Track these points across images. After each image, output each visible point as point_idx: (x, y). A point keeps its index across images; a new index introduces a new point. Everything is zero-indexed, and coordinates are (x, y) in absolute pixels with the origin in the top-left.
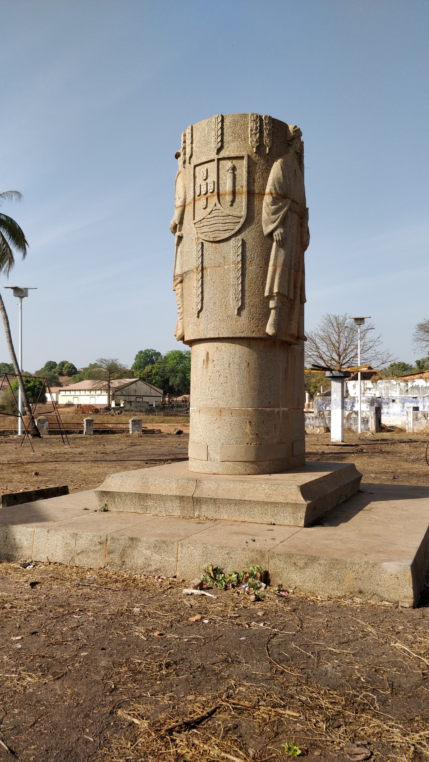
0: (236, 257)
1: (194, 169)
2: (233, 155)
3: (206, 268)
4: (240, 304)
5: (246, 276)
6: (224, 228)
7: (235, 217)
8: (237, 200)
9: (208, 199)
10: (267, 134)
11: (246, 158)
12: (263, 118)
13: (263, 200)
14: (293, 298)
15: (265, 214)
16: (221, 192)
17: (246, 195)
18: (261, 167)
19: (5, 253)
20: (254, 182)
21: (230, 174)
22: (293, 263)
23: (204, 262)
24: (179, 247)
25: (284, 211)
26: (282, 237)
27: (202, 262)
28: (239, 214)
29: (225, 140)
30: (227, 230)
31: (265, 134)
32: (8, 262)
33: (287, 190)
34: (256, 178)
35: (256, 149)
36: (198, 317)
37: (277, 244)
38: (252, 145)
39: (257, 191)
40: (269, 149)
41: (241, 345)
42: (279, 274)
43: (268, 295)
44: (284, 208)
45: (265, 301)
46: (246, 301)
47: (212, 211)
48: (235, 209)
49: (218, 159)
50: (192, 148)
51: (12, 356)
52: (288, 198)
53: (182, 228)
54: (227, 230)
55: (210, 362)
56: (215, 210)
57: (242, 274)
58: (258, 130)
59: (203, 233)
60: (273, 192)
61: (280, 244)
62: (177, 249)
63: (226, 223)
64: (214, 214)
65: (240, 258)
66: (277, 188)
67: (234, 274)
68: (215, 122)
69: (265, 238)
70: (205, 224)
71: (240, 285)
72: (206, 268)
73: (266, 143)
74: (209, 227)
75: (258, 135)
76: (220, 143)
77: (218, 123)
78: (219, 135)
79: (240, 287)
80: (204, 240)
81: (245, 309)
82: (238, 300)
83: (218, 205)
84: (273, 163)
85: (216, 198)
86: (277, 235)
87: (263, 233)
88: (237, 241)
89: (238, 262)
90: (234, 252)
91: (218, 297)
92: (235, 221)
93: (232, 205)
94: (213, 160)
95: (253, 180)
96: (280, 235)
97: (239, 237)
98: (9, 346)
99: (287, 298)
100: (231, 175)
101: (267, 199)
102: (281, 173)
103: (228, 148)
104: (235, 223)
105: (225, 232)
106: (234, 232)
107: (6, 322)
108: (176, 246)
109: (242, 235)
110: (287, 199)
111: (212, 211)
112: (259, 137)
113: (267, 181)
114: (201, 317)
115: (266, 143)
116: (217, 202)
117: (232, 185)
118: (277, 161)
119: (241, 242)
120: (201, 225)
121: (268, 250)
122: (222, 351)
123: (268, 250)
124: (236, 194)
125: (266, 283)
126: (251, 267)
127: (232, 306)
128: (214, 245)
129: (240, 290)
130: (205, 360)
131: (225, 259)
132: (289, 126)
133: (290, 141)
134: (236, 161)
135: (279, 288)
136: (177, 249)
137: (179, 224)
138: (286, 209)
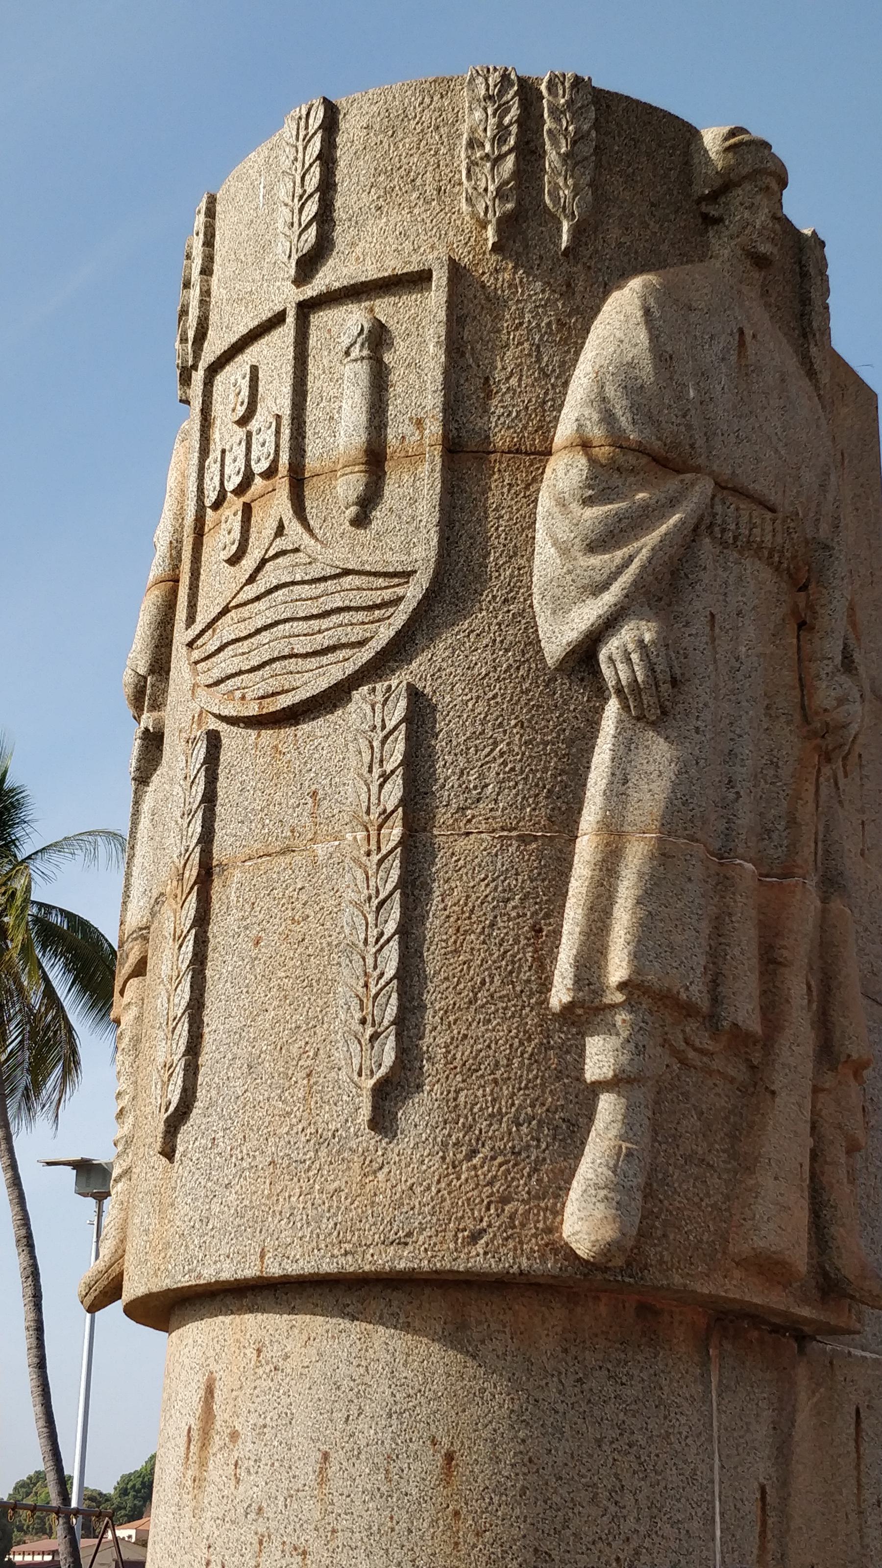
0: (374, 789)
2: (371, 272)
4: (389, 1058)
5: (431, 892)
7: (376, 574)
8: (391, 489)
10: (565, 158)
11: (440, 278)
12: (543, 88)
13: (537, 479)
14: (755, 1025)
16: (312, 463)
17: (438, 460)
18: (528, 317)
19: (49, 1040)
20: (489, 395)
22: (745, 818)
23: (219, 834)
24: (151, 788)
25: (663, 529)
26: (651, 669)
27: (207, 838)
28: (395, 561)
29: (340, 214)
31: (552, 157)
32: (58, 1071)
33: (689, 427)
34: (498, 375)
35: (499, 231)
36: (168, 1152)
37: (625, 707)
38: (474, 215)
39: (501, 438)
40: (577, 232)
41: (407, 1327)
42: (641, 875)
43: (566, 998)
44: (664, 517)
45: (557, 1039)
46: (428, 1040)
48: (379, 536)
51: (42, 1423)
52: (697, 469)
53: (165, 691)
55: (217, 1441)
56: (276, 556)
57: (403, 884)
58: (512, 141)
59: (217, 683)
60: (596, 433)
61: (640, 706)
62: (137, 803)
64: (269, 577)
65: (394, 792)
66: (618, 412)
67: (362, 885)
68: (293, 141)
71: (394, 944)
73: (556, 199)
75: (510, 162)
76: (313, 230)
77: (307, 141)
78: (309, 191)
79: (392, 952)
80: (219, 717)
81: (419, 1087)
82: (374, 1037)
83: (294, 527)
84: (604, 300)
86: (617, 657)
88: (380, 698)
89: (386, 816)
90: (367, 759)
92: (377, 597)
93: (361, 521)
94: (278, 319)
95: (479, 382)
96: (635, 657)
97: (399, 680)
98: (35, 1383)
99: (712, 1021)
101: (561, 473)
102: (643, 336)
103: (353, 244)
105: (324, 660)
106: (365, 655)
107: (30, 1292)
108: (132, 785)
110: (688, 477)
112: (517, 174)
113: (566, 384)
114: (184, 1154)
115: (556, 199)
117: (363, 418)
118: (620, 287)
119: (403, 703)
121: (570, 743)
122: (288, 1366)
123: (570, 743)
124: (389, 466)
125: (557, 933)
126: (462, 842)
127: (343, 1075)
128: (268, 736)
129: (390, 972)
130: (195, 1434)
131: (317, 804)
132: (703, 132)
133: (714, 197)
134: (392, 299)
135: (637, 956)
136: (137, 803)
138: (676, 518)
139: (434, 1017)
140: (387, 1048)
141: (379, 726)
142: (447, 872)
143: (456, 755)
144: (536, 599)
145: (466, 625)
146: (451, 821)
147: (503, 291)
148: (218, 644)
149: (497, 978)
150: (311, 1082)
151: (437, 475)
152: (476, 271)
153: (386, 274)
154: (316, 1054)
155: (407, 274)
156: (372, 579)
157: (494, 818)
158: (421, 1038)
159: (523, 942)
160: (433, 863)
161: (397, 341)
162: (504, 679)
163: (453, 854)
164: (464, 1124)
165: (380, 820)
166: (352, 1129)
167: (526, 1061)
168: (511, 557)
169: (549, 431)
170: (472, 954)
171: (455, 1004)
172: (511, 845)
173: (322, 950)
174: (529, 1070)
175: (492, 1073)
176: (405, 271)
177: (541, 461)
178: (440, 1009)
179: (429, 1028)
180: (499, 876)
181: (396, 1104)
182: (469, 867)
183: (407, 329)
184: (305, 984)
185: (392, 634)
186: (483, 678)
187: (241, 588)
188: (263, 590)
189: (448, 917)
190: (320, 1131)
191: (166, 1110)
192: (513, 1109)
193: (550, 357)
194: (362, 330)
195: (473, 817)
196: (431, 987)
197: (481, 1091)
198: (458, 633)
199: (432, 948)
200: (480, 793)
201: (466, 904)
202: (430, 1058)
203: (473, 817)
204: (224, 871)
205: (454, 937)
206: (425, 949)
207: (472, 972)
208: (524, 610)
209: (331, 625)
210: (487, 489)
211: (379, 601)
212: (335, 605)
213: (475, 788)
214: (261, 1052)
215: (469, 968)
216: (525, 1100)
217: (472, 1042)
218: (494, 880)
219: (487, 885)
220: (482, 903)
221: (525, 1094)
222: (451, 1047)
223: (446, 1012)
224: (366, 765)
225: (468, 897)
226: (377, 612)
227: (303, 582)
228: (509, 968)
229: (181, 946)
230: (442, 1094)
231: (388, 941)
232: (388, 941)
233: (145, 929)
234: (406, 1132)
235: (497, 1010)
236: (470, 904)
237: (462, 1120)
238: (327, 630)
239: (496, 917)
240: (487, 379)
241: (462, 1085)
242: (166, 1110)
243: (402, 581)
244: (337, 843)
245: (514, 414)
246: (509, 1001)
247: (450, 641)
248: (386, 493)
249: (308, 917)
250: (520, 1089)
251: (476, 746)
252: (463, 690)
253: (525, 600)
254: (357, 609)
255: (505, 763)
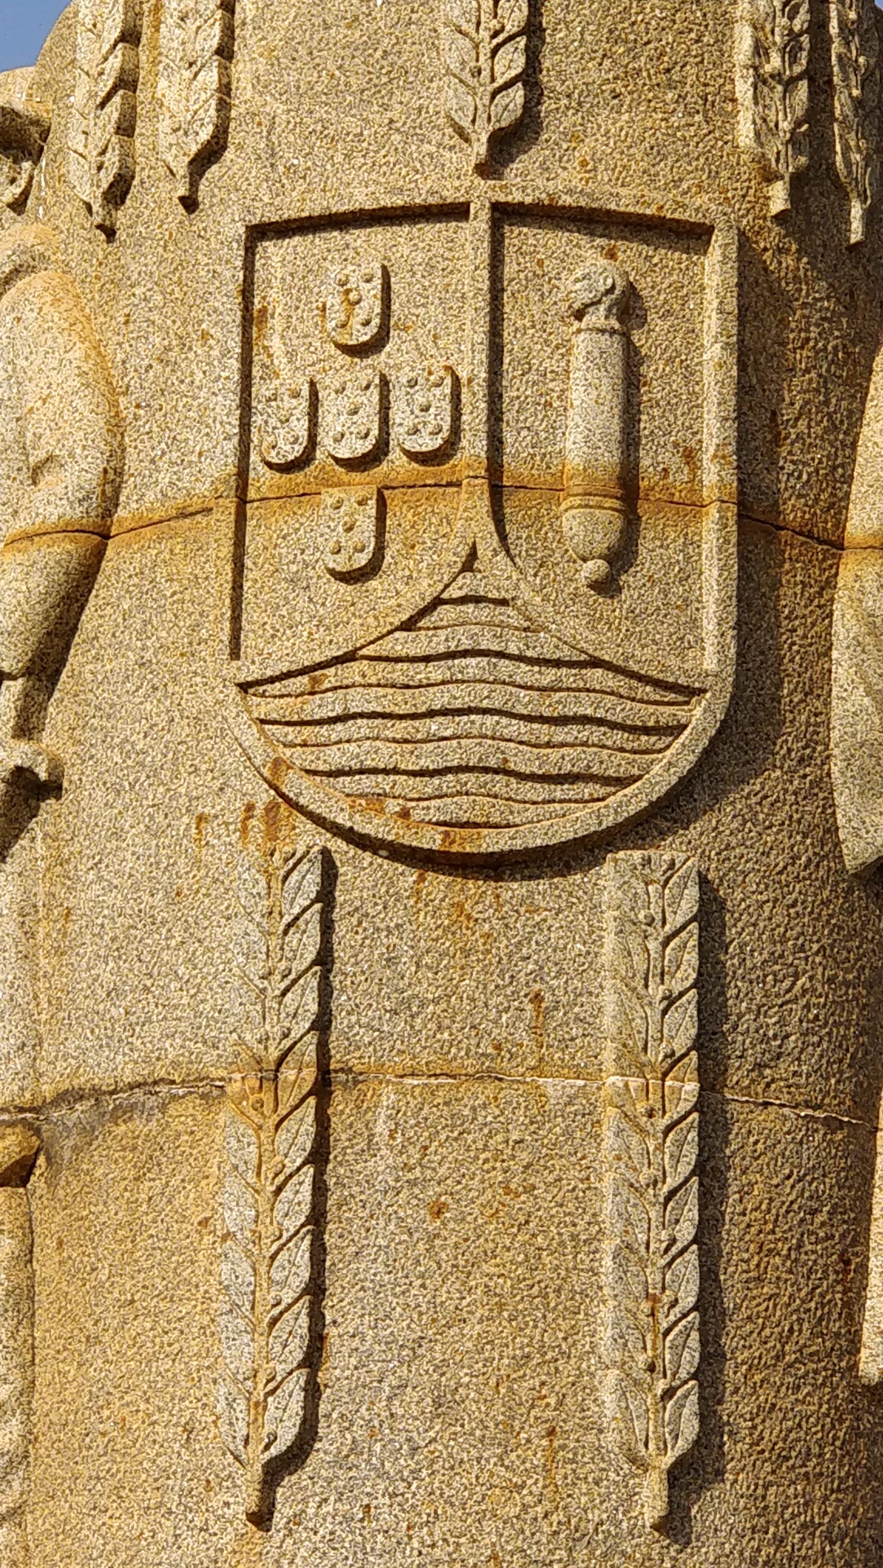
1: (250, 251)
3: (356, 1079)
4: (690, 1428)
5: (724, 1186)
6: (554, 755)
8: (646, 545)
9: (393, 507)
10: (858, 103)
13: (830, 584)
15: (860, 699)
18: (814, 332)
21: (604, 340)
23: (340, 1022)
30: (572, 778)
31: (841, 105)
34: (788, 414)
40: (869, 217)
47: (438, 602)
49: (496, 207)
50: (225, 89)
54: (572, 778)
56: (463, 600)
63: (563, 721)
69: (850, 891)
70: (357, 701)
71: (692, 1256)
72: (356, 1079)
73: (848, 163)
74: (400, 729)
78: (511, 28)
81: (720, 1473)
82: (668, 1393)
85: (484, 505)
87: (837, 844)
91: (484, 1342)
92: (650, 715)
100: (613, 346)
103: (576, 138)
104: (646, 730)
105: (559, 792)
109: (693, 832)
111: (438, 602)
113: (854, 445)
114: (297, 1519)
116: (487, 544)
119: (692, 892)
120: (330, 704)
127: (610, 1439)
129: (688, 1299)
137: (28, 672)
139: (735, 1373)
140: (686, 1411)
141: (658, 917)
142: (743, 1159)
143: (751, 982)
144: (836, 768)
145: (758, 787)
146: (747, 1082)
147: (787, 284)
148: (339, 710)
149: (806, 1325)
150: (556, 1444)
151: (733, 550)
152: (757, 242)
153: (648, 212)
154: (560, 1403)
155: (678, 221)
156: (634, 683)
157: (798, 1086)
158: (720, 1402)
159: (832, 1277)
160: (727, 1143)
161: (652, 316)
162: (804, 878)
163: (750, 1132)
164: (774, 1534)
165: (666, 1065)
166: (625, 1525)
167: (838, 1452)
168: (806, 695)
169: (840, 513)
170: (778, 1287)
171: (760, 1358)
172: (816, 1131)
173: (562, 1244)
174: (842, 1466)
175: (804, 1465)
176: (676, 216)
177: (834, 556)
178: (743, 1363)
179: (730, 1388)
180: (805, 1175)
181: (688, 1495)
182: (769, 1155)
183: (666, 301)
184: (535, 1291)
185: (674, 780)
186: (780, 873)
187: (390, 632)
188: (442, 649)
189: (749, 1226)
190: (573, 1521)
191: (267, 1447)
192: (826, 1520)
193: (839, 403)
194: (613, 287)
195: (773, 1081)
196: (730, 1326)
197: (792, 1490)
198: (748, 797)
199: (732, 1269)
200: (780, 1047)
201: (769, 1211)
202: (731, 1431)
203: (773, 1081)
204: (356, 1082)
205: (756, 1258)
206: (722, 1271)
207: (778, 1313)
208: (821, 779)
209: (570, 739)
210: (776, 585)
211: (651, 723)
212: (581, 711)
213: (775, 1037)
214: (459, 1385)
215: (775, 1305)
216: (837, 1508)
217: (781, 1415)
218: (799, 1181)
219: (793, 1187)
220: (787, 1212)
221: (837, 1500)
222: (758, 1421)
223: (750, 1367)
224: (640, 976)
225: (771, 1200)
226: (644, 738)
227: (520, 658)
228: (819, 1313)
229: (279, 1190)
230: (748, 1487)
231: (681, 1253)
232: (681, 1253)
233: (30, 1110)
234: (703, 1538)
235: (807, 1373)
236: (774, 1211)
237: (772, 1530)
238: (563, 745)
239: (802, 1235)
240: (774, 413)
241: (770, 1478)
242: (267, 1447)
243: (681, 699)
244: (581, 1083)
245: (805, 477)
246: (820, 1361)
247: (739, 806)
248: (643, 551)
249: (534, 1188)
250: (832, 1491)
251: (775, 975)
252: (758, 885)
253: (823, 764)
254: (614, 726)
255: (807, 1007)
